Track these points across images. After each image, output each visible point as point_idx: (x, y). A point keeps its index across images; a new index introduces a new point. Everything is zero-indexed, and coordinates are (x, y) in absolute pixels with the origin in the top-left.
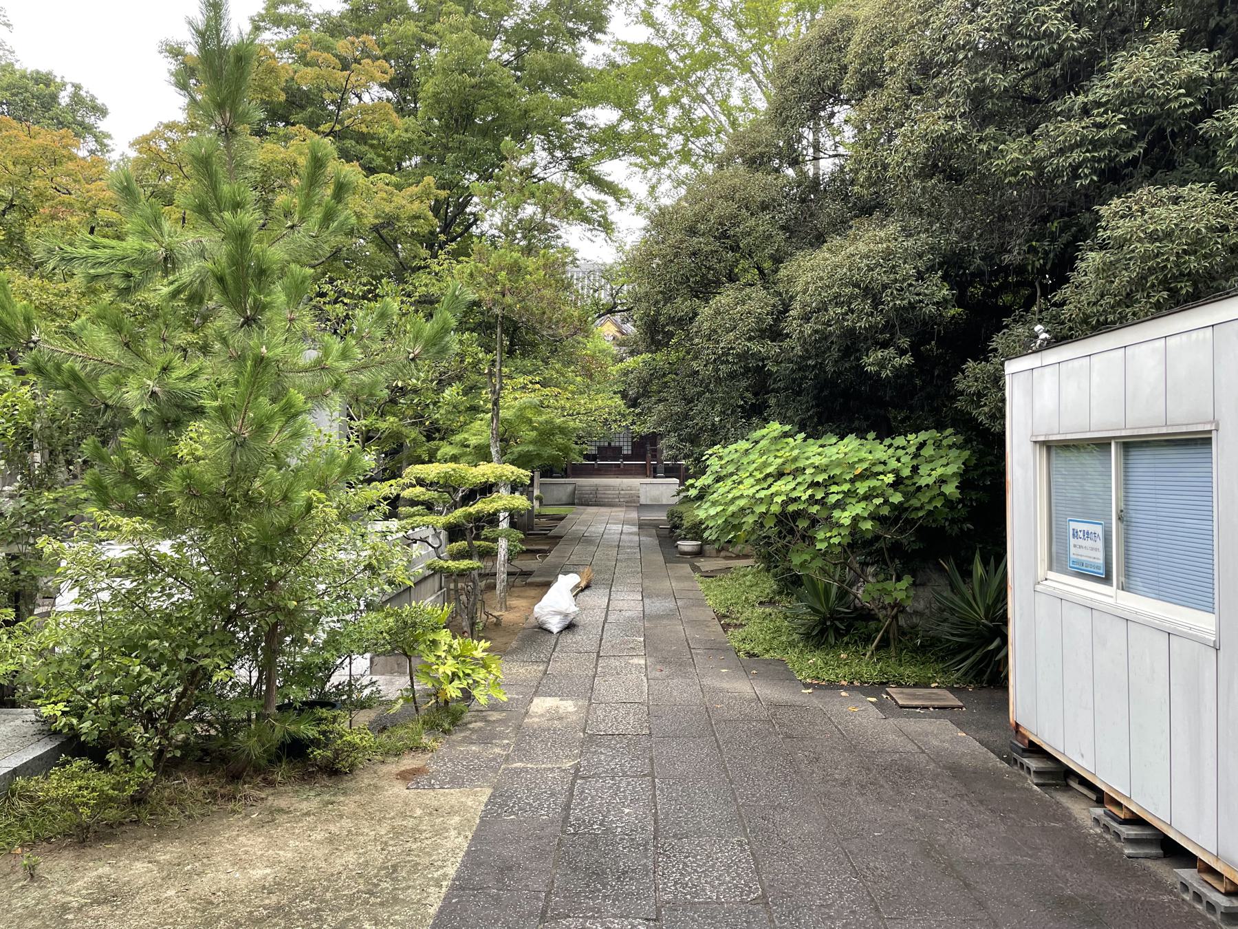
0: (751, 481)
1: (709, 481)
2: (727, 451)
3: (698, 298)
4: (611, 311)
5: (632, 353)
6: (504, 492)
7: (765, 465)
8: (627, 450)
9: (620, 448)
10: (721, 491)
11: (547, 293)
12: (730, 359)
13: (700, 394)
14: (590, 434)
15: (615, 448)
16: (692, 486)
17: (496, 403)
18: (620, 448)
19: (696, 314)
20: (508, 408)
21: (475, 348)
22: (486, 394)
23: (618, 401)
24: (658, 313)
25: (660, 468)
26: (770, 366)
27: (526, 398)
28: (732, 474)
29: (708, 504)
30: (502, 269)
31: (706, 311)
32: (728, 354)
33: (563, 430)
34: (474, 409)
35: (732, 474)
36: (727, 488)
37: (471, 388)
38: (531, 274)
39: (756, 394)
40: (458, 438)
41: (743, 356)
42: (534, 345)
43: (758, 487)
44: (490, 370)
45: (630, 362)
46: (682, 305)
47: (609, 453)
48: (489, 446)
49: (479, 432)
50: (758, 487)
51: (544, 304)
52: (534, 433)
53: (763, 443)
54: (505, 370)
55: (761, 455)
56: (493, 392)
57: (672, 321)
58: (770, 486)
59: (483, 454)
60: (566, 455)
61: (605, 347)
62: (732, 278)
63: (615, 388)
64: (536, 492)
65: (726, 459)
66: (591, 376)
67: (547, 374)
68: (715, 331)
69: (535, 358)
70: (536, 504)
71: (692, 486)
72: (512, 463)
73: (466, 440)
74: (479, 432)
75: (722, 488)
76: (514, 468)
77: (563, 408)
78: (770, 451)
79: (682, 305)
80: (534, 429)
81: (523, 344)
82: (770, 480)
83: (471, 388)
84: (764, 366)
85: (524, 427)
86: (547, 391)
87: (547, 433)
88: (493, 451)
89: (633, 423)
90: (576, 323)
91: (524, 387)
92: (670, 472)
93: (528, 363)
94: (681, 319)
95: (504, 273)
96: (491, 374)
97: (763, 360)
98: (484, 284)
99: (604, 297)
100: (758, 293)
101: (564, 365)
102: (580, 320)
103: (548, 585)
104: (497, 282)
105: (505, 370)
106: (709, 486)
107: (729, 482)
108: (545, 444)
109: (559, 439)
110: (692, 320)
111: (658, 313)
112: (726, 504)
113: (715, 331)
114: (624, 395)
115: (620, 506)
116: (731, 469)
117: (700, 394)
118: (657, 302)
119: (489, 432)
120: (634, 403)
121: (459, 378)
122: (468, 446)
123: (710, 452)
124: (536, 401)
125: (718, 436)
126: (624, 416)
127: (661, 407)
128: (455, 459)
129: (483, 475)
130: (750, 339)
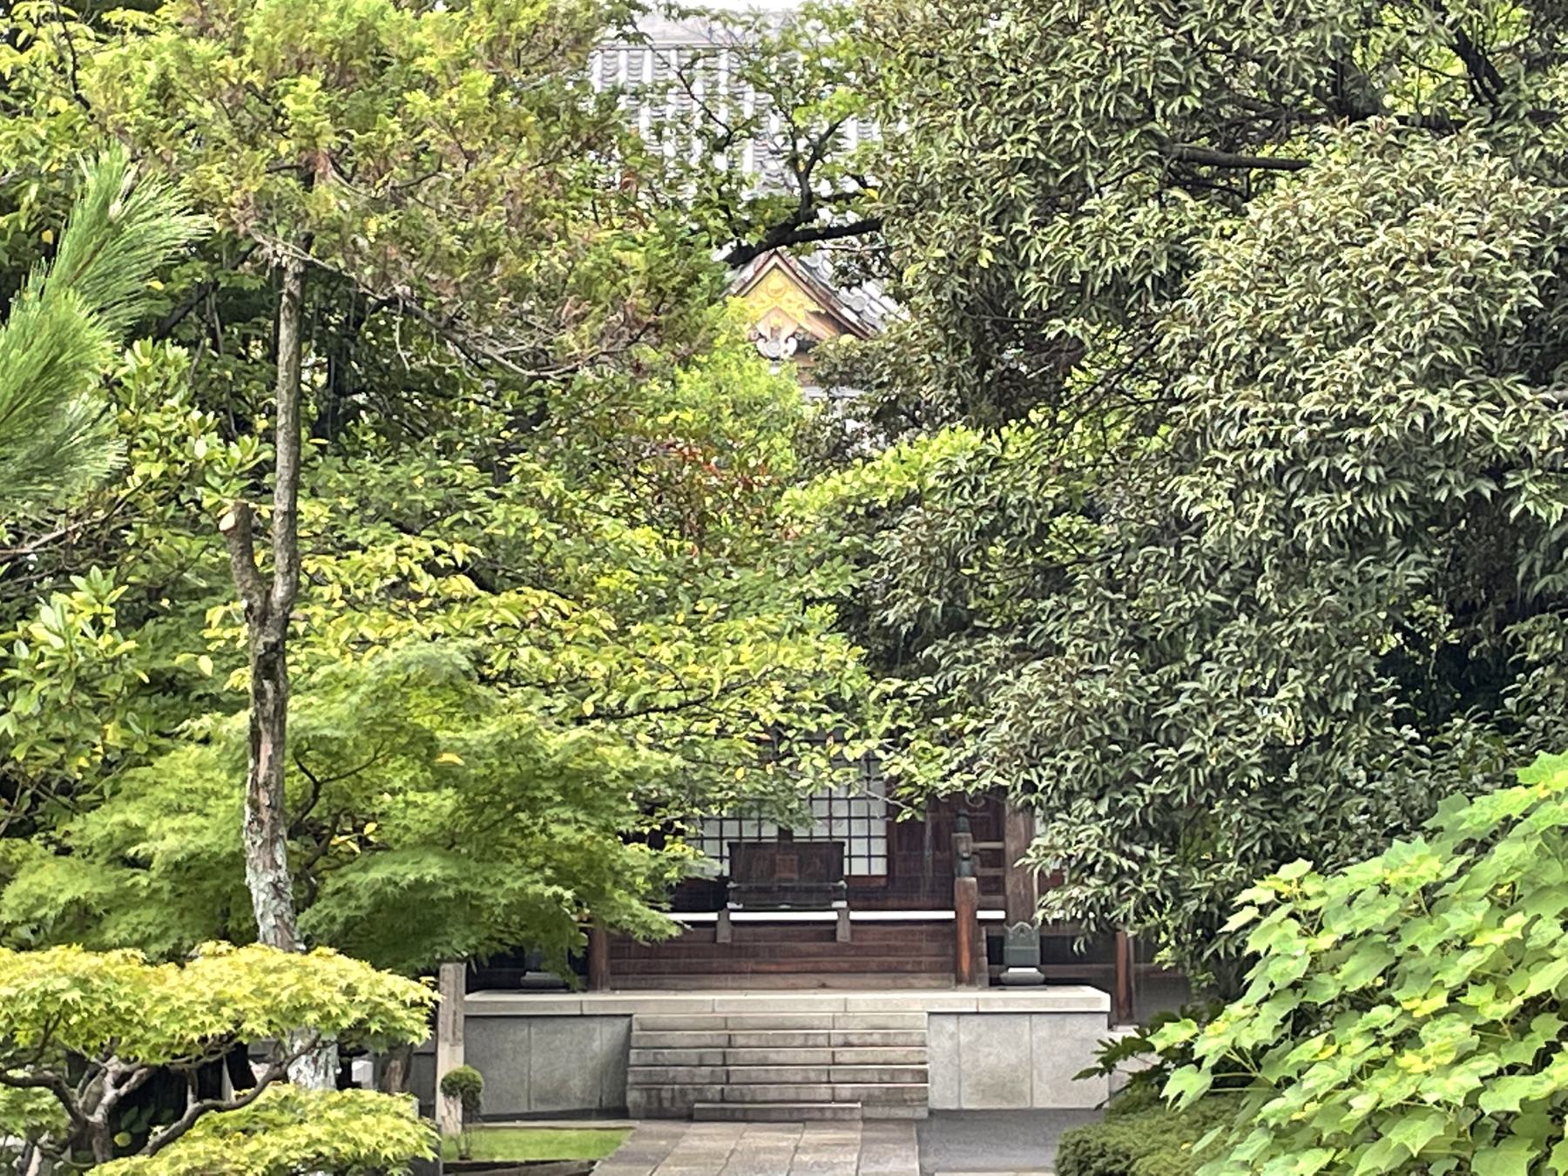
0: (1458, 1031)
1: (1263, 1031)
2: (1338, 887)
3: (1198, 188)
4: (791, 231)
5: (892, 419)
6: (309, 1079)
7: (1519, 956)
8: (866, 859)
9: (834, 851)
10: (1320, 1078)
11: (512, 167)
12: (1346, 463)
13: (1210, 622)
14: (696, 794)
15: (812, 846)
16: (1183, 1055)
17: (270, 666)
18: (834, 851)
19: (1184, 264)
20: (327, 688)
21: (176, 415)
22: (226, 623)
23: (839, 651)
24: (1011, 253)
25: (1022, 940)
26: (1530, 497)
27: (408, 644)
28: (1363, 1001)
29: (1258, 1141)
30: (302, 67)
31: (1229, 252)
32: (1339, 446)
33: (579, 787)
34: (172, 693)
35: (1363, 1001)
36: (1346, 1066)
37: (154, 594)
38: (430, 85)
39: (1464, 613)
40: (96, 826)
41: (1404, 456)
42: (442, 387)
43: (1488, 1063)
44: (245, 514)
45: (887, 467)
46: (1124, 220)
47: (788, 875)
48: (237, 862)
49: (192, 797)
50: (1488, 1063)
51: (491, 219)
52: (445, 801)
53: (1506, 852)
54: (309, 509)
55: (1503, 906)
56: (260, 616)
57: (1073, 294)
58: (1543, 1060)
59: (210, 904)
60: (591, 895)
61: (760, 388)
62: (1348, 101)
63: (813, 583)
64: (450, 1061)
65: (1340, 928)
66: (699, 528)
67: (502, 518)
68: (1273, 340)
69: (447, 449)
70: (449, 1111)
71: (1183, 1055)
72: (350, 941)
73: (136, 834)
74: (192, 797)
75: (1322, 1063)
76: (357, 970)
77: (576, 684)
78: (1542, 891)
79: (1124, 220)
80: (444, 777)
81: (392, 383)
82: (1546, 1028)
83: (154, 594)
84: (1502, 495)
85: (399, 771)
86: (502, 606)
87: (505, 801)
88: (258, 883)
89: (896, 739)
90: (639, 299)
91: (401, 587)
92: (1061, 960)
93: (415, 472)
94: (1118, 287)
95: (309, 85)
96: (249, 531)
97: (1497, 472)
98: (222, 129)
99: (758, 170)
100: (1469, 168)
101: (576, 477)
102: (654, 288)
103: (235, 712)
104: (275, 122)
105: (309, 509)
106: (1260, 1051)
107: (1355, 1044)
108: (492, 853)
109: (566, 829)
110: (1170, 286)
111: (1011, 253)
112: (1340, 1141)
113: (1273, 340)
114: (853, 616)
115: (836, 1120)
116: (1359, 973)
117: (1210, 622)
118: (1006, 210)
119: (239, 797)
120: (893, 654)
121: (103, 548)
122: (143, 864)
123: (1262, 892)
124: (455, 653)
125: (1297, 818)
126: (849, 707)
127: (1029, 680)
128: (80, 924)
129: (217, 1005)
130: (1436, 377)
